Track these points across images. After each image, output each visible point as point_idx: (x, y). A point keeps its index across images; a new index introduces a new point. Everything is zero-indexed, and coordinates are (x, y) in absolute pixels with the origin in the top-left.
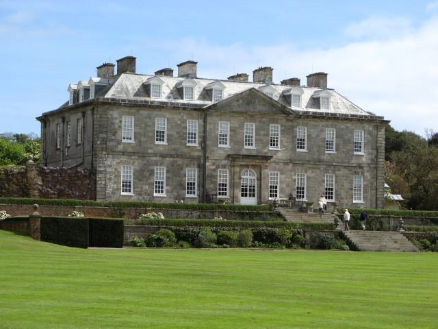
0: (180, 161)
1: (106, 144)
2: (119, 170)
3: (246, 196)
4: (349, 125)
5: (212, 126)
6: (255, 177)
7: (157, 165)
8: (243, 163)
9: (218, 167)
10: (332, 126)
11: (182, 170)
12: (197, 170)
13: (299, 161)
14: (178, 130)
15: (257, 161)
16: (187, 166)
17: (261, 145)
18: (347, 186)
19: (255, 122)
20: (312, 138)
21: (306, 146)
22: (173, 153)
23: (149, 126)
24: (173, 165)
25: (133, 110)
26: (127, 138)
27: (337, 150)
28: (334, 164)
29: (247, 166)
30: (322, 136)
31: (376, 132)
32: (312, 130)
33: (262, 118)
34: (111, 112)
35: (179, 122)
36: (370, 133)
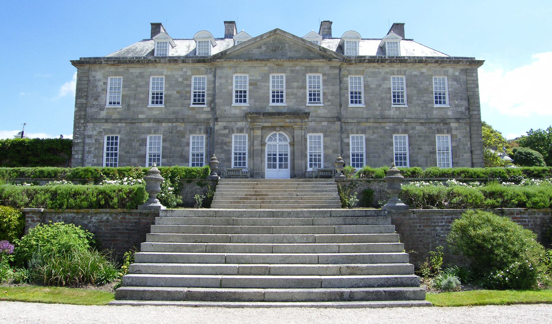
0: (181, 126)
1: (85, 111)
2: (101, 141)
3: (275, 167)
4: (424, 70)
5: (223, 81)
6: (287, 143)
7: (150, 133)
8: (266, 124)
9: (232, 131)
10: (399, 72)
11: (183, 137)
12: (205, 136)
13: (353, 118)
14: (178, 89)
15: (287, 120)
16: (191, 132)
17: (294, 100)
18: (426, 148)
19: (285, 73)
20: (371, 89)
21: (363, 100)
22: (171, 116)
23: (140, 87)
24: (171, 132)
25: (121, 68)
26: (114, 103)
27: (409, 102)
28: (406, 120)
29: (273, 128)
30: (385, 86)
31: (465, 77)
32: (369, 79)
33: (296, 65)
34: (93, 74)
35: (180, 80)
36: (456, 79)
